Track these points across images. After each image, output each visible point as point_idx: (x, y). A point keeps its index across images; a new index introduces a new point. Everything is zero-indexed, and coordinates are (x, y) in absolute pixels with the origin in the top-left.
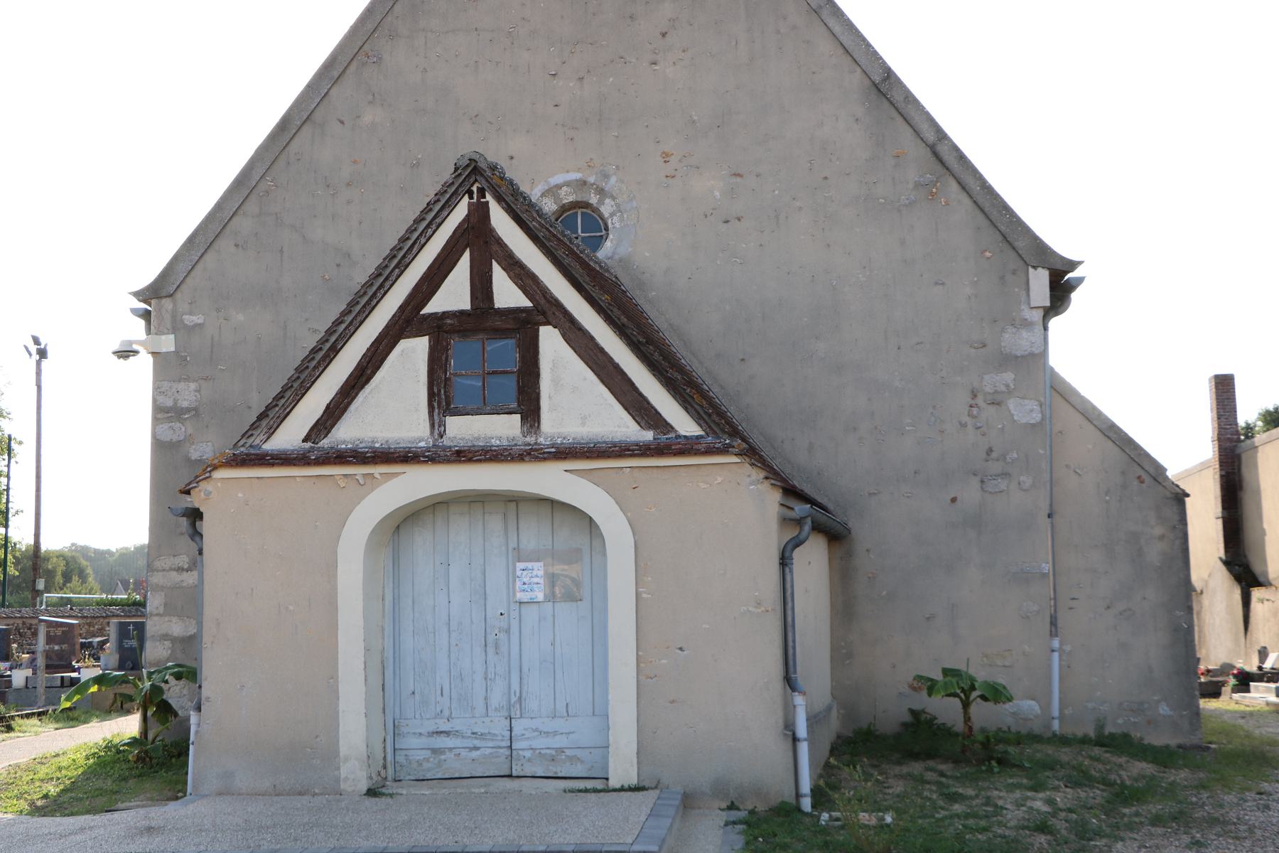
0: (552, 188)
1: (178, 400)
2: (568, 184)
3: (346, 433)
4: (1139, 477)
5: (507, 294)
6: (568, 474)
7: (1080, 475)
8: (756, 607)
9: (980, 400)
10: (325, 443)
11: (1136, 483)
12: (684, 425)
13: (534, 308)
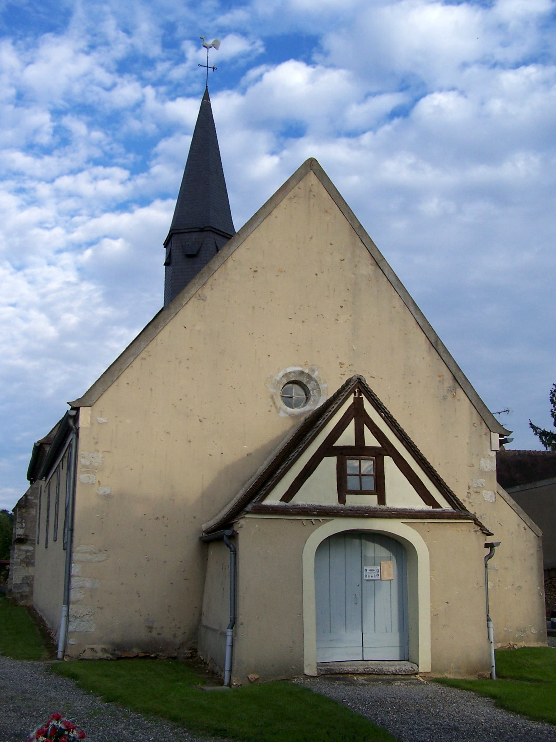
0: (287, 373)
1: (92, 462)
2: (294, 372)
3: (300, 499)
4: (524, 527)
5: (371, 441)
6: (403, 524)
7: (501, 525)
8: (476, 585)
9: (471, 491)
10: (290, 504)
11: (523, 529)
12: (445, 506)
13: (382, 448)
